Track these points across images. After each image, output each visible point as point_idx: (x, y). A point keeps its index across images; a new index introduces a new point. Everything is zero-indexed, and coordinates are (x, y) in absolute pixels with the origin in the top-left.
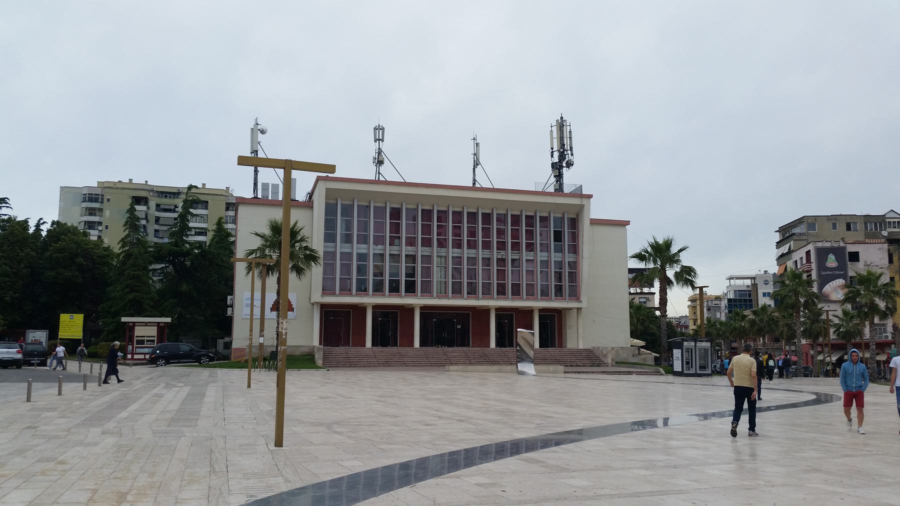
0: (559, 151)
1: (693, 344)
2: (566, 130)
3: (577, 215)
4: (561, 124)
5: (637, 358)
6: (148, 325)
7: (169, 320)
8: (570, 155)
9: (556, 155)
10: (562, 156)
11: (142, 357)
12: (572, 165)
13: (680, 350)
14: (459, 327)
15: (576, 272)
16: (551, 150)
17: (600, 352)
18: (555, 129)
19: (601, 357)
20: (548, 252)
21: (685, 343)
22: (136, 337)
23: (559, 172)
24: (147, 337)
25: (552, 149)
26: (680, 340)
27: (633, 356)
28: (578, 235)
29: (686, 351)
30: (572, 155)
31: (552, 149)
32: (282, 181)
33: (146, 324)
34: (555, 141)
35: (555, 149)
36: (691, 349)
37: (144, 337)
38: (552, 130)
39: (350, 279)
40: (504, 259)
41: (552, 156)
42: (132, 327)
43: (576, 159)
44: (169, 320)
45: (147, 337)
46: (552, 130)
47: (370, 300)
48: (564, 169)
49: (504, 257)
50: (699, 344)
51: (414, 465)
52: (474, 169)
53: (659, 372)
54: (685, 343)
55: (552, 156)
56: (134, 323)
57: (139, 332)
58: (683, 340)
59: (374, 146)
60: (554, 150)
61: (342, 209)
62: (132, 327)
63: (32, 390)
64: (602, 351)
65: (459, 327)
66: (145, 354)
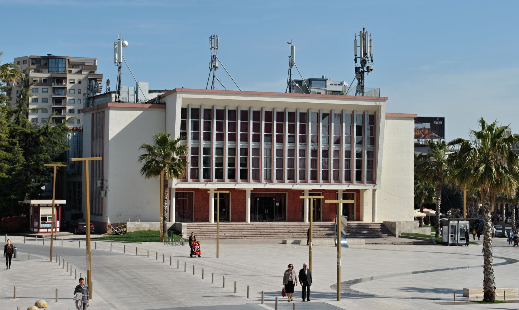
0: (361, 58)
1: (456, 222)
2: (368, 39)
3: (375, 113)
4: (363, 36)
5: (418, 230)
6: (49, 206)
7: (64, 202)
8: (370, 62)
9: (359, 60)
10: (363, 62)
11: (45, 230)
12: (372, 70)
13: (447, 227)
14: (277, 204)
15: (372, 160)
16: (355, 57)
17: (390, 225)
18: (358, 38)
19: (391, 230)
20: (351, 144)
21: (451, 222)
22: (41, 215)
23: (361, 76)
24: (49, 215)
25: (356, 55)
26: (447, 219)
27: (415, 228)
28: (375, 129)
29: (451, 228)
30: (372, 61)
31: (356, 55)
32: (139, 87)
33: (47, 206)
34: (358, 49)
35: (358, 56)
36: (455, 226)
37: (47, 215)
38: (356, 40)
39: (198, 169)
40: (316, 150)
41: (356, 62)
42: (37, 208)
43: (374, 66)
44: (64, 202)
45: (49, 215)
46: (356, 40)
47: (213, 186)
48: (366, 73)
49: (316, 149)
50: (460, 222)
51: (469, 233)
52: (290, 70)
53: (432, 243)
54: (451, 222)
55: (356, 62)
56: (39, 205)
57: (43, 212)
58: (449, 220)
59: (210, 53)
60: (357, 57)
61: (196, 121)
62: (37, 208)
63: (52, 259)
64: (391, 225)
65: (277, 204)
66: (47, 228)
